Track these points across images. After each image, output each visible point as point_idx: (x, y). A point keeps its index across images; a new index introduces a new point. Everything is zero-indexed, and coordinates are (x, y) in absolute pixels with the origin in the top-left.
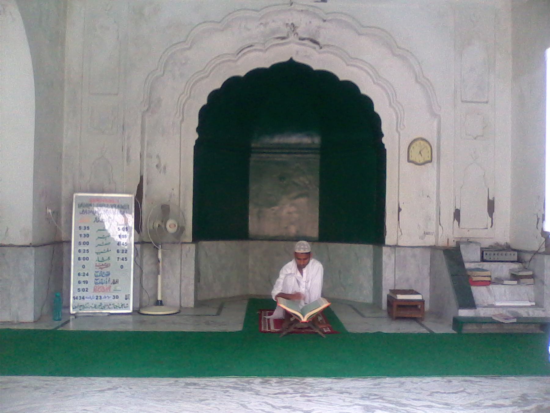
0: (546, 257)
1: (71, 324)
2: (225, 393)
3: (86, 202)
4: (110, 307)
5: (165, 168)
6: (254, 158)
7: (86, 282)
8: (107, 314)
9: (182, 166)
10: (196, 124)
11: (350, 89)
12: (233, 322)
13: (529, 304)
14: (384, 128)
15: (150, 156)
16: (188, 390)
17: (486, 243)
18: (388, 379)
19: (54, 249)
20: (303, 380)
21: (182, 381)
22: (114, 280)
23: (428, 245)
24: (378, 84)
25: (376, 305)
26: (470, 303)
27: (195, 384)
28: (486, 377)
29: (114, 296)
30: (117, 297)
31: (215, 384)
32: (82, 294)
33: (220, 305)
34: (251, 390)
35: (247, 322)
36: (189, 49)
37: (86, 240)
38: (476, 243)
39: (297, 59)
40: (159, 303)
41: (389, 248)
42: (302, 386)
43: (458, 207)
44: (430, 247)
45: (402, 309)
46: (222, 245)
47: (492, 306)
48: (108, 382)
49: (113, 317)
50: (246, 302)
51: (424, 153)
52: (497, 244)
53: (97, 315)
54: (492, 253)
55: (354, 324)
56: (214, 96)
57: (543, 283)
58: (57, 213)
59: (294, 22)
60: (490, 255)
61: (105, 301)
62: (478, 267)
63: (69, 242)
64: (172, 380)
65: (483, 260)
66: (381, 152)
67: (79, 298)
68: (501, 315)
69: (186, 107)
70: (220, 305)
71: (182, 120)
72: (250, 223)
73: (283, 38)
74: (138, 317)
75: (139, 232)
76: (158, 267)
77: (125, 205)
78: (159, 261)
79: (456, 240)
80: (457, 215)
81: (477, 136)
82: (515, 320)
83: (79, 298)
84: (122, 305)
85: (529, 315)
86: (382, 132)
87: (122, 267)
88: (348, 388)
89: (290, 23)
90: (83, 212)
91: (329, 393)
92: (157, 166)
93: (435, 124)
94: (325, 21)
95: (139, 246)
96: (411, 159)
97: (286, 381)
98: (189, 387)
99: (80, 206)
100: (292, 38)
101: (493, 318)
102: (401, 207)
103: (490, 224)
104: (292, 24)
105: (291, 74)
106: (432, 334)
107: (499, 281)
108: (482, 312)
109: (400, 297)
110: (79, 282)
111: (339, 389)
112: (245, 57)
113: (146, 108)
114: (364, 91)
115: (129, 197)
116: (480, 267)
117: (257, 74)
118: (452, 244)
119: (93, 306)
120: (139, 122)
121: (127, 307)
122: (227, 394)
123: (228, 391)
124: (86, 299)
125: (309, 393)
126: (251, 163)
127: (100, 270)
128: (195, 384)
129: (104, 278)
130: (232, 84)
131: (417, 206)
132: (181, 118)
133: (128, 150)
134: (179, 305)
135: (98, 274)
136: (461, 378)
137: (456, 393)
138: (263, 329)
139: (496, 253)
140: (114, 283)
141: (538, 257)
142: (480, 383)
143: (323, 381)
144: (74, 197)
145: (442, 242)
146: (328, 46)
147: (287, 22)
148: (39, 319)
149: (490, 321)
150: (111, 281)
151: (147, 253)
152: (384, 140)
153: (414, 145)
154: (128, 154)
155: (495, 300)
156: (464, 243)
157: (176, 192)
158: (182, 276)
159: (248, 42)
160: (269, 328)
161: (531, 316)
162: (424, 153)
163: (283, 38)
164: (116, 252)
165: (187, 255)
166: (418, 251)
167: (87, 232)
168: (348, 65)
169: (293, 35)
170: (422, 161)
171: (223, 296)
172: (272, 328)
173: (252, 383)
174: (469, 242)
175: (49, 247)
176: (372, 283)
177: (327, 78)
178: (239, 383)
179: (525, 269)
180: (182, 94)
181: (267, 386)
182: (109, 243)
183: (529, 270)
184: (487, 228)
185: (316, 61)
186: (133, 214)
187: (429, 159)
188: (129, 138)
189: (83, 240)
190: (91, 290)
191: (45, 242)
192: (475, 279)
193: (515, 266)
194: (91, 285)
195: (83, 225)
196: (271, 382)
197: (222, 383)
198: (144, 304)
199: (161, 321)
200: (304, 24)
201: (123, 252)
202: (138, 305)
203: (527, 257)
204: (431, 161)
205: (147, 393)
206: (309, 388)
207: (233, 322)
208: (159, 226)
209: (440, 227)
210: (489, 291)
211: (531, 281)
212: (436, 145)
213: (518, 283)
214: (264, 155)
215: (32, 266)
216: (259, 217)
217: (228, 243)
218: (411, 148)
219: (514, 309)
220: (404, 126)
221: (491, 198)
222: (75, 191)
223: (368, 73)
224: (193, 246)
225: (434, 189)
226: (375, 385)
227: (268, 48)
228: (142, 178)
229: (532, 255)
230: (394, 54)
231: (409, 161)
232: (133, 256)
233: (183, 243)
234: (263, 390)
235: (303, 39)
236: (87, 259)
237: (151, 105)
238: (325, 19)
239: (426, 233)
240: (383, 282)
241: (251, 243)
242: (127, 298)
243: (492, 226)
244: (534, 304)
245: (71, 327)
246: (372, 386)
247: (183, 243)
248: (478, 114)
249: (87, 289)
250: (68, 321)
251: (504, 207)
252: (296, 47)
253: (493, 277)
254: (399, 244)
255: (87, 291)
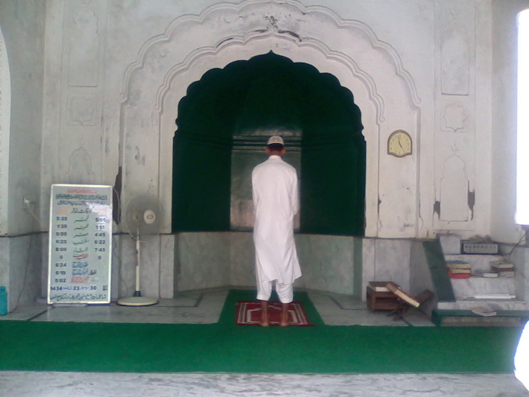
0: (527, 250)
1: (48, 314)
2: (188, 390)
3: (65, 193)
4: (88, 297)
5: (144, 159)
6: (235, 150)
7: (63, 273)
8: (84, 305)
9: (161, 159)
10: (175, 116)
11: (330, 81)
12: (209, 314)
13: (509, 297)
14: (365, 120)
15: (128, 147)
16: (151, 387)
17: (467, 236)
18: (360, 376)
19: (32, 239)
20: (273, 376)
21: (147, 376)
22: (92, 271)
23: (409, 237)
24: (357, 76)
25: (355, 298)
26: (450, 297)
27: (159, 380)
28: (463, 374)
29: (92, 287)
30: (95, 288)
31: (180, 380)
32: (60, 285)
33: (200, 296)
34: (216, 387)
35: (224, 315)
36: (169, 41)
37: (64, 230)
38: (456, 235)
39: (277, 52)
40: (138, 294)
41: (369, 240)
42: (270, 383)
43: (438, 200)
44: (410, 239)
45: (385, 302)
46: (203, 237)
47: (472, 299)
48: (71, 377)
49: (90, 308)
50: (227, 293)
51: (403, 145)
52: (478, 236)
53: (74, 305)
54: (474, 245)
55: (331, 316)
56: (194, 88)
57: (523, 275)
58: (35, 204)
59: (272, 15)
60: (470, 247)
61: (82, 292)
62: (457, 259)
63: (47, 232)
64: (135, 376)
65: (463, 253)
66: (360, 145)
67: (56, 288)
68: (481, 308)
69: (165, 99)
70: (200, 296)
71: (161, 114)
72: (232, 215)
73: (263, 31)
74: (116, 308)
75: (117, 223)
76: (136, 258)
77: (103, 196)
78: (137, 252)
79: (436, 232)
80: (437, 207)
81: (458, 128)
82: (495, 314)
83: (56, 288)
84: (100, 296)
85: (509, 308)
86: (361, 124)
87: (100, 258)
88: (318, 385)
89: (269, 16)
90: (62, 203)
91: (297, 391)
92: (136, 157)
93: (415, 116)
94: (304, 14)
95: (117, 237)
96: (390, 151)
97: (254, 377)
98: (153, 383)
99: (58, 196)
100: (272, 30)
101: (473, 311)
102: (380, 199)
103: (471, 217)
104: (272, 17)
105: (270, 67)
106: (411, 327)
107: (479, 274)
108: (462, 305)
109: (379, 289)
110: (57, 273)
111: (308, 386)
112: (223, 51)
113: (125, 100)
114: (343, 84)
115: (107, 188)
116: (460, 260)
117: (236, 67)
118: (432, 236)
119: (71, 297)
120: (118, 113)
121: (105, 298)
122: (191, 391)
123: (192, 388)
124: (63, 290)
125: (276, 391)
126: (233, 156)
127: (78, 261)
128: (159, 380)
129: (82, 269)
130: (212, 76)
131: (396, 199)
132: (160, 110)
133: (107, 141)
134: (157, 295)
135: (76, 265)
136: (437, 375)
137: (429, 391)
138: (239, 322)
139: (476, 245)
140: (92, 274)
141: (519, 250)
142: (456, 381)
143: (293, 377)
144: (52, 187)
145: (422, 235)
146: (308, 38)
147: (267, 15)
148: (15, 309)
149: (469, 314)
150: (89, 272)
151: (126, 243)
152: (364, 132)
153: (393, 137)
154: (106, 145)
155: (477, 293)
156: (443, 235)
157: (155, 183)
158: (161, 266)
159: (228, 35)
160: (246, 321)
161: (511, 309)
162: (403, 145)
163: (263, 31)
164: (94, 242)
165: (166, 247)
166: (397, 243)
167: (64, 223)
168: (328, 58)
169: (272, 27)
170: (402, 153)
171: (204, 286)
172: (249, 320)
173: (220, 379)
174: (449, 234)
175: (26, 237)
176: (352, 275)
177: (307, 71)
178: (205, 379)
179: (506, 262)
180: (162, 86)
181: (234, 382)
182: (87, 234)
183: (510, 263)
184: (467, 221)
185: (296, 53)
186: (111, 205)
187: (409, 151)
188: (107, 129)
189: (61, 230)
190: (68, 280)
191: (23, 232)
192: (455, 271)
193: (495, 259)
194: (68, 276)
195: (60, 216)
196: (239, 378)
197: (187, 380)
198: (123, 295)
199: (138, 311)
200: (283, 16)
201: (100, 243)
202: (116, 296)
203: (508, 250)
204: (411, 154)
205: (107, 390)
206: (277, 385)
207: (209, 314)
208: (137, 217)
209: (420, 219)
210: (469, 284)
211: (512, 273)
212: (415, 137)
213: (499, 276)
214: (245, 147)
215: (7, 257)
216: (240, 209)
217: (210, 234)
218: (391, 141)
219: (493, 302)
220: (383, 118)
221: (471, 191)
222: (54, 183)
223: (349, 67)
224: (172, 238)
225: (414, 181)
226: (347, 382)
227: (248, 41)
228: (120, 169)
229: (512, 247)
230: (374, 48)
231: (389, 153)
232: (110, 247)
233: (161, 234)
234: (230, 388)
235: (283, 32)
236: (65, 249)
237: (130, 97)
238: (304, 12)
239: (406, 226)
240: (363, 275)
241: (233, 234)
242: (105, 288)
243: (472, 218)
244: (514, 297)
245: (49, 317)
246: (343, 384)
247: (161, 234)
248: (459, 106)
249: (65, 279)
250: (45, 312)
251: (483, 199)
252: (274, 40)
253: (474, 269)
254: (381, 235)
255: (64, 282)
